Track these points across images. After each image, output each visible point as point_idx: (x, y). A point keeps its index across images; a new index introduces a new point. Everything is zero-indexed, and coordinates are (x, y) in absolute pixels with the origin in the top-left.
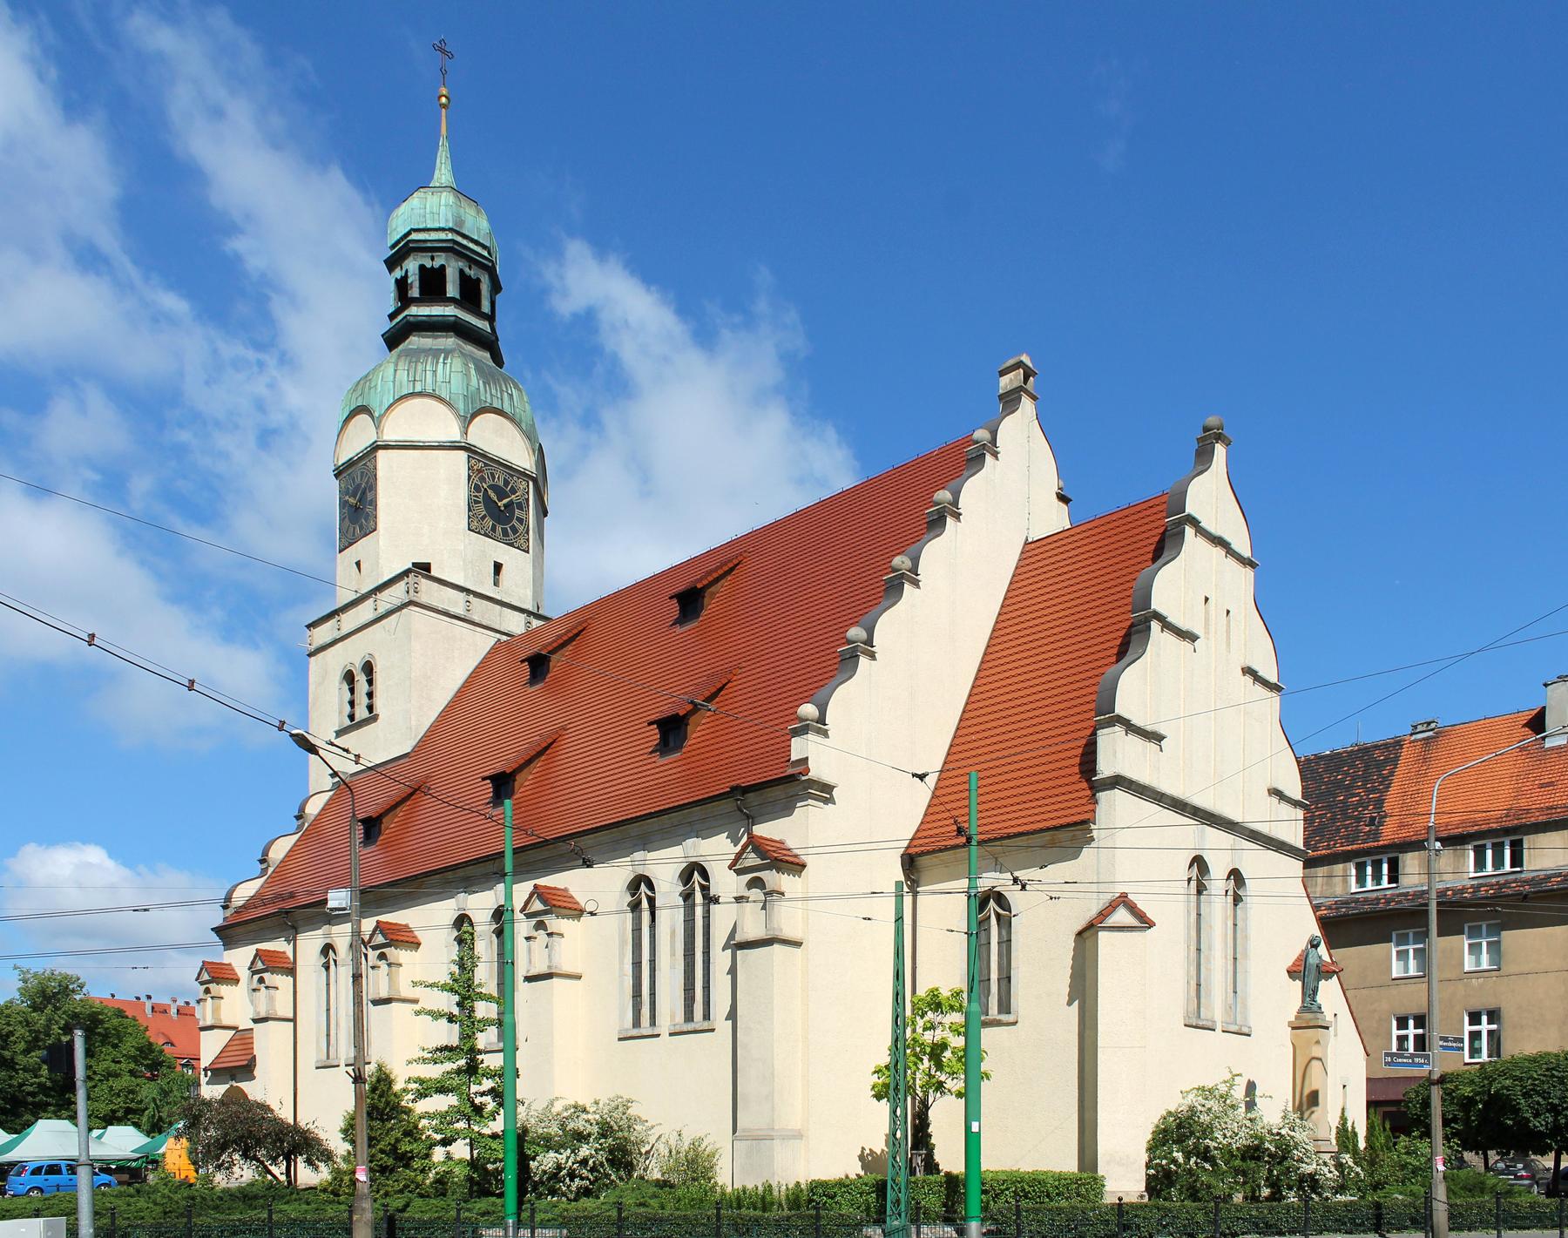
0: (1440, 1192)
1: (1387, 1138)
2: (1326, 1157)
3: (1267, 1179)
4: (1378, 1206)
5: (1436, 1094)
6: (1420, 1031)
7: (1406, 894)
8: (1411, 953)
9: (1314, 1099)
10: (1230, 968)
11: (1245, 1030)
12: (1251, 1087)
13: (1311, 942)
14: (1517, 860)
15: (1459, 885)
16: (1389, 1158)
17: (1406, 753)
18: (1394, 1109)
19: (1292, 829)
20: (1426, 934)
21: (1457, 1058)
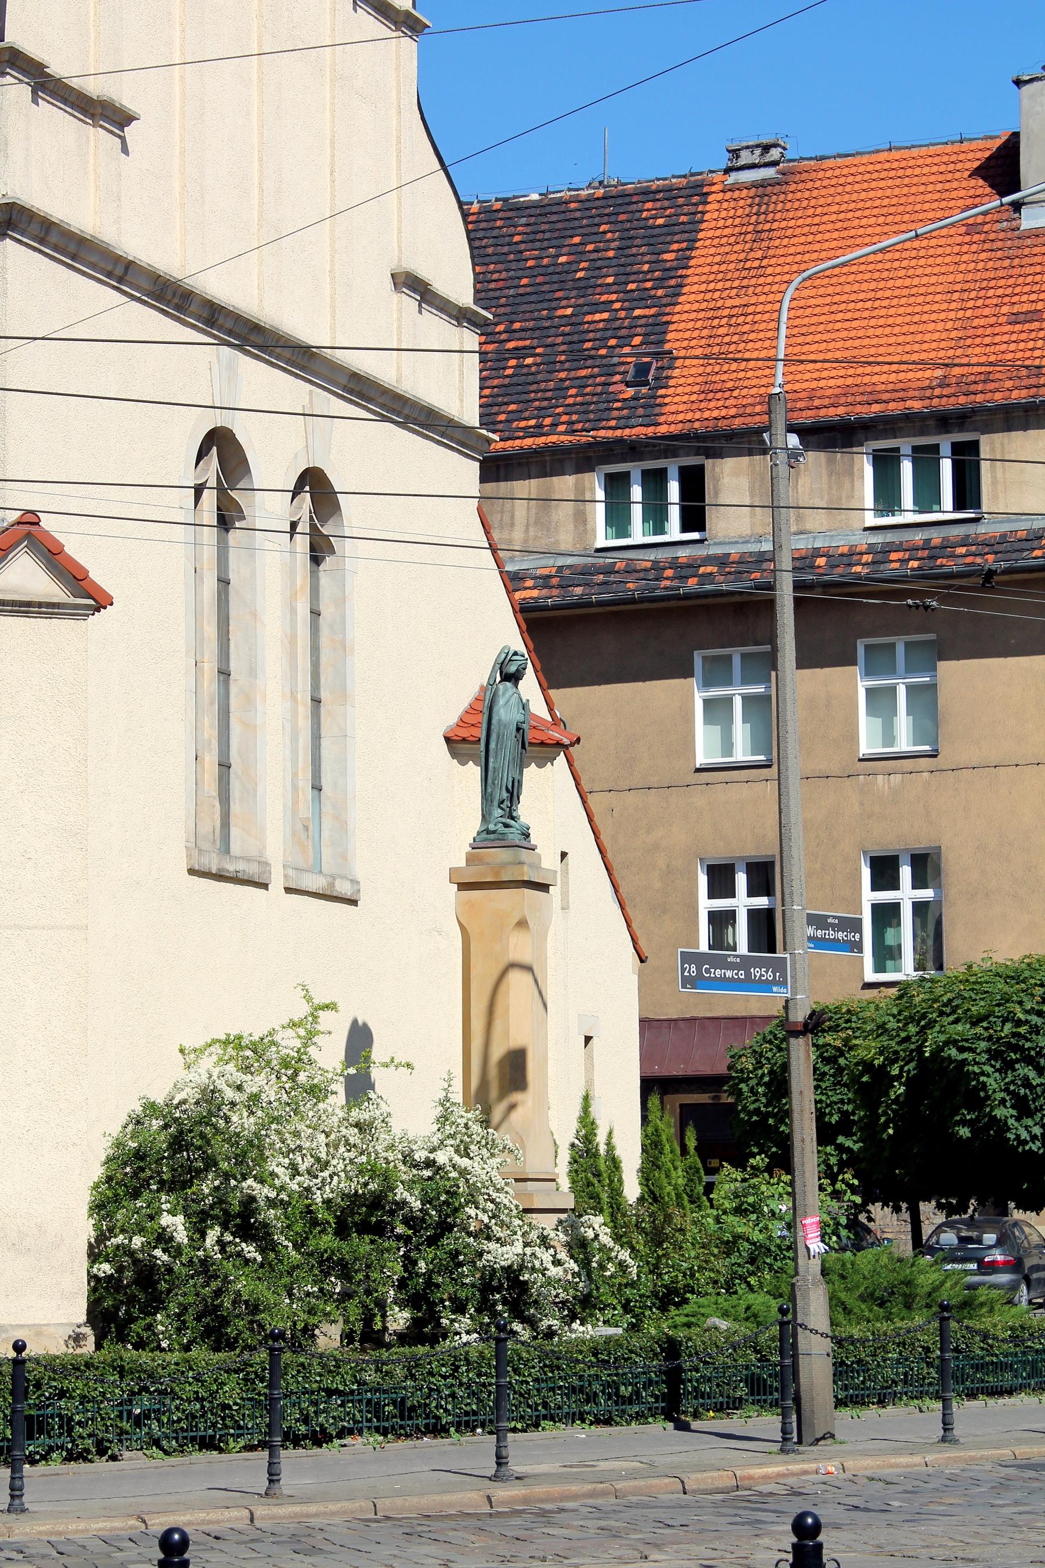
0: (815, 1309)
1: (691, 1172)
2: (547, 1223)
3: (402, 1285)
4: (671, 1348)
5: (802, 1057)
6: (762, 902)
7: (722, 561)
8: (738, 702)
9: (515, 1071)
10: (304, 723)
11: (343, 888)
12: (360, 1039)
13: (502, 665)
14: (967, 493)
15: (841, 543)
16: (695, 1224)
17: (715, 213)
18: (704, 1098)
19: (454, 386)
20: (771, 661)
21: (841, 974)
